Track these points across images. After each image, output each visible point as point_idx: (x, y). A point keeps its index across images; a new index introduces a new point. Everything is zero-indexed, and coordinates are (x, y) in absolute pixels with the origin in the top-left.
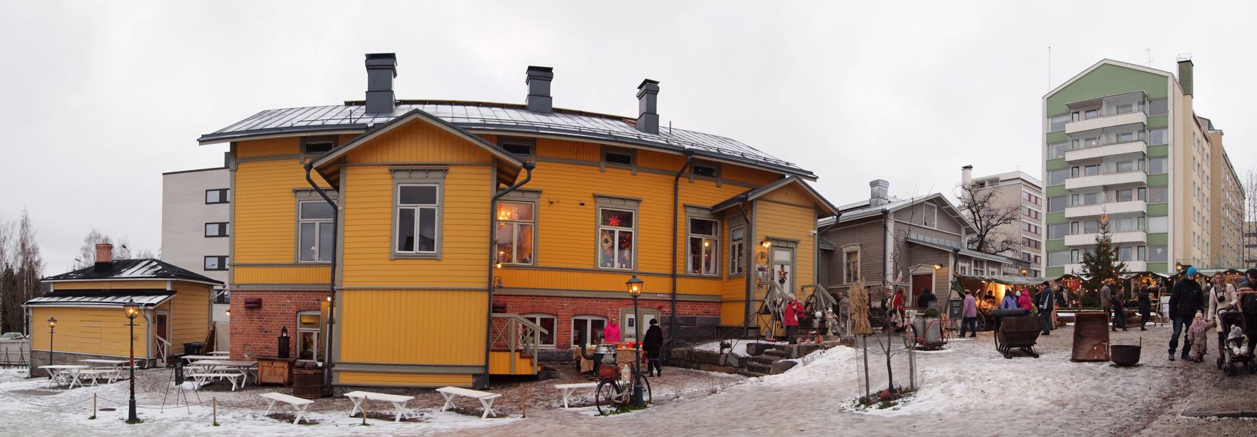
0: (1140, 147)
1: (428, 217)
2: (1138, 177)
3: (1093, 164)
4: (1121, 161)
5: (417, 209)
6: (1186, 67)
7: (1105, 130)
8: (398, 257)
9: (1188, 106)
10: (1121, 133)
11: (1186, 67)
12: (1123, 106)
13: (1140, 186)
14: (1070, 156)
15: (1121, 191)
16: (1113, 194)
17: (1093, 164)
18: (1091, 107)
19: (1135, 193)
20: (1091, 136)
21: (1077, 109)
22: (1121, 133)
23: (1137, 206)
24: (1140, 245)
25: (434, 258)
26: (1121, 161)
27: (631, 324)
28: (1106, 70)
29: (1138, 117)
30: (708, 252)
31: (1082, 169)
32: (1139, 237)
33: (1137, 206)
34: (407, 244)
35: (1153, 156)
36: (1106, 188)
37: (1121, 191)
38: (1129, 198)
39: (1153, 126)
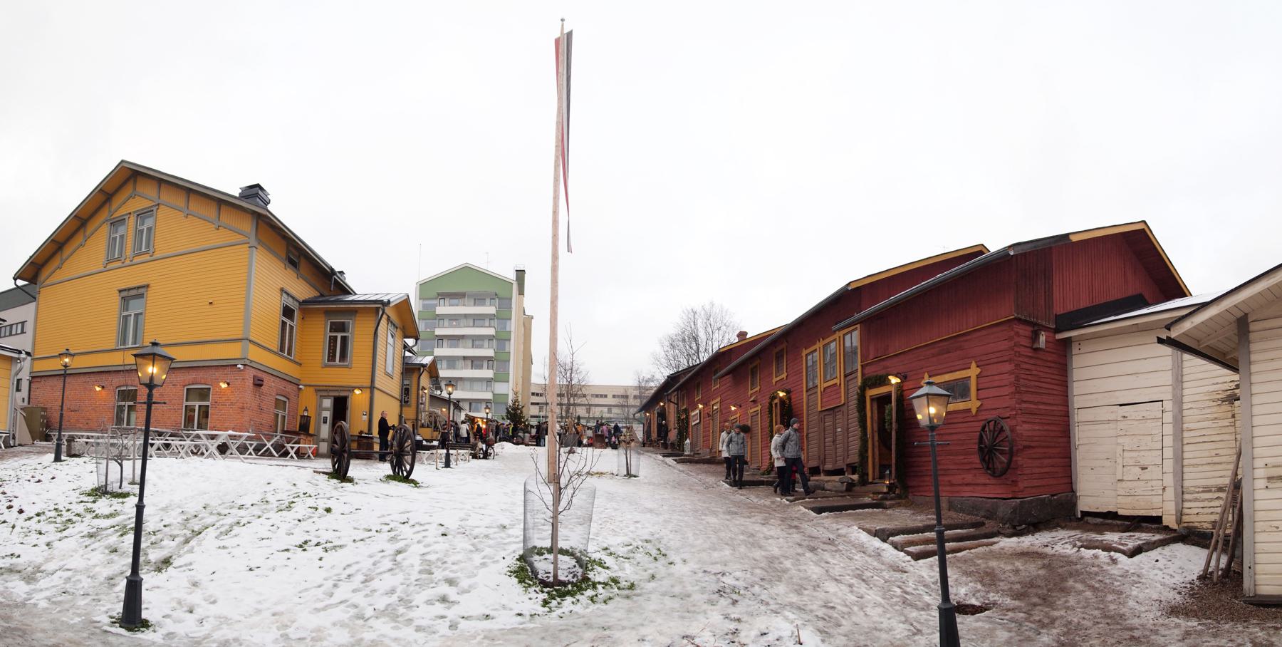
0: (491, 331)
1: (344, 339)
2: (489, 352)
3: (455, 340)
4: (476, 340)
5: (339, 335)
6: (520, 274)
7: (466, 316)
8: (326, 366)
9: (520, 303)
10: (477, 319)
11: (520, 274)
12: (479, 299)
13: (489, 359)
14: (438, 332)
15: (475, 362)
16: (469, 363)
17: (455, 340)
18: (457, 296)
19: (485, 364)
20: (454, 318)
21: (443, 296)
22: (477, 319)
23: (488, 373)
24: (488, 401)
25: (347, 367)
26: (476, 340)
27: (325, 419)
28: (467, 271)
29: (491, 310)
30: (833, 355)
31: (445, 342)
32: (489, 396)
33: (488, 373)
34: (332, 356)
35: (501, 339)
36: (465, 358)
37: (475, 362)
38: (481, 367)
39: (502, 316)
